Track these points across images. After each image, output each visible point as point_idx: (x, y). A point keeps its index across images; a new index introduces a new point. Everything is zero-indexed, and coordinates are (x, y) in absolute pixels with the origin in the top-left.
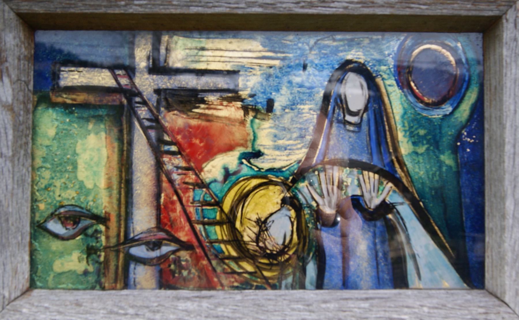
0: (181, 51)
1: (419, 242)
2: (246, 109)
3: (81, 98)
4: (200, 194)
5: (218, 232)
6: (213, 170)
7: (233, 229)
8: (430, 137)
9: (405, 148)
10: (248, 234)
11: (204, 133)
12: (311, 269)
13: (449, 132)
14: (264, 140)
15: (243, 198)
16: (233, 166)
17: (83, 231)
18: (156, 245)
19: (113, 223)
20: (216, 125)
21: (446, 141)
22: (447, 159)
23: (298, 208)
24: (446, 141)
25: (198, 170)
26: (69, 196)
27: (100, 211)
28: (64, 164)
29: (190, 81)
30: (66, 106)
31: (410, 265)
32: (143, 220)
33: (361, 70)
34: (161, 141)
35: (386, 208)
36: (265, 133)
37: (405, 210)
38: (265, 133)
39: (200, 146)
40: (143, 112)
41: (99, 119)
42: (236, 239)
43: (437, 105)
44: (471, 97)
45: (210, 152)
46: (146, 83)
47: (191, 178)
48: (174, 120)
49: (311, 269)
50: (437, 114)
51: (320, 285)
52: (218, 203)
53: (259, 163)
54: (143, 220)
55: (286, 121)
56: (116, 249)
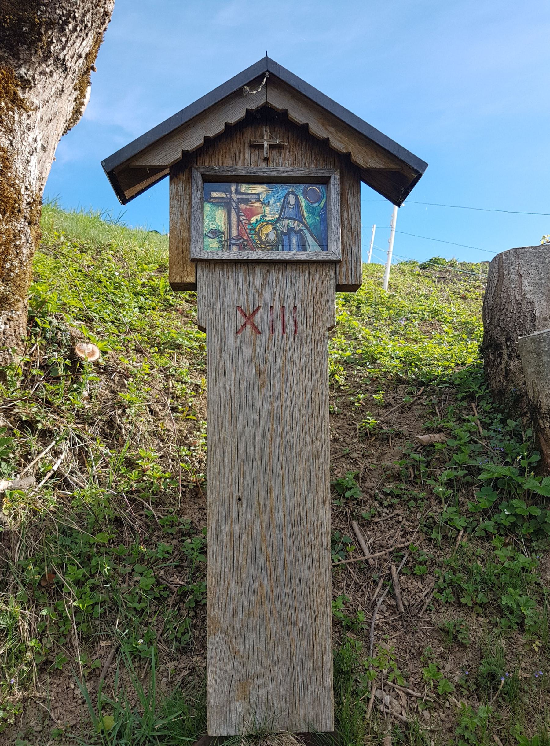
0: (244, 188)
1: (310, 240)
2: (262, 204)
3: (217, 200)
4: (250, 226)
5: (254, 237)
6: (253, 220)
7: (259, 236)
8: (311, 211)
9: (306, 215)
10: (263, 237)
11: (250, 210)
12: (280, 247)
13: (318, 210)
14: (267, 212)
15: (261, 227)
16: (259, 219)
17: (218, 236)
18: (238, 240)
19: (226, 234)
20: (254, 208)
21: (317, 213)
22: (317, 218)
23: (277, 231)
24: (317, 213)
25: (249, 220)
26: (213, 227)
27: (222, 231)
28: (145, 291)
29: (247, 196)
30: (212, 202)
31: (307, 246)
32: (234, 233)
33: (293, 193)
34: (239, 212)
35: (301, 230)
36: (267, 211)
37: (306, 231)
38: (267, 211)
39: (251, 213)
40: (234, 204)
41: (222, 206)
42: (260, 239)
43: (314, 203)
44: (324, 201)
45: (252, 216)
46: (234, 196)
47: (247, 222)
48: (242, 206)
49: (280, 247)
50: (314, 206)
51: (283, 250)
52: (255, 229)
53: (266, 218)
54: (234, 233)
55: (273, 207)
56: (227, 241)
